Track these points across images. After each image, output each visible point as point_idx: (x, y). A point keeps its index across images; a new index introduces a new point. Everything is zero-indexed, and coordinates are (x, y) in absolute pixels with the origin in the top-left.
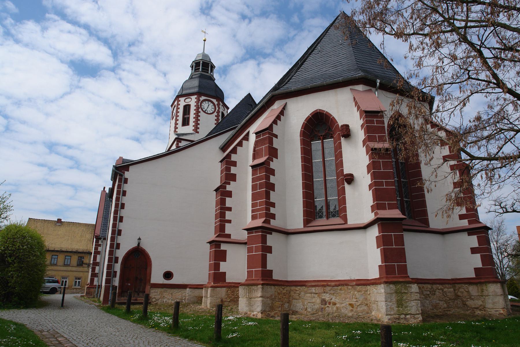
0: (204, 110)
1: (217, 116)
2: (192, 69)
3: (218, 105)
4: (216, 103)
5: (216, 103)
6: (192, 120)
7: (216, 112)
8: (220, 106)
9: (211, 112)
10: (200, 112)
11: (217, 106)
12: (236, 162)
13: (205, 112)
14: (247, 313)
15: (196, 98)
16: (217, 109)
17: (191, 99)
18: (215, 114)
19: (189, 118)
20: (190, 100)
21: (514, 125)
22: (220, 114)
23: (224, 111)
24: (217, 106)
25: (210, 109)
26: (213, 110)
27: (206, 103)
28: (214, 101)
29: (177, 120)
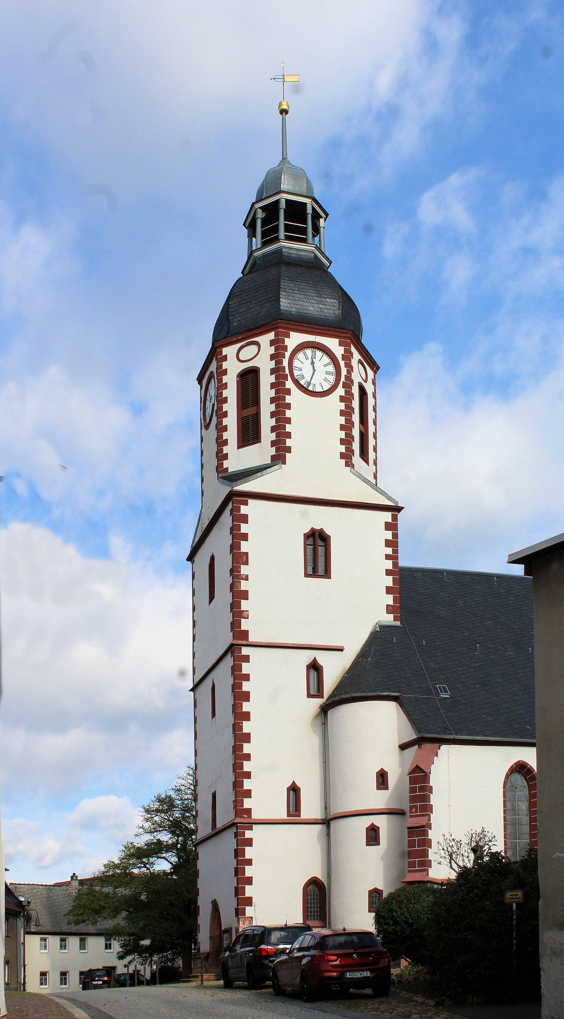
0: (302, 382)
1: (346, 399)
2: (252, 233)
3: (347, 357)
4: (339, 351)
5: (339, 351)
8: (354, 362)
9: (327, 387)
10: (288, 392)
11: (342, 363)
13: (304, 390)
15: (272, 343)
16: (344, 371)
17: (257, 344)
20: (254, 348)
22: (355, 390)
23: (366, 381)
24: (342, 363)
26: (332, 379)
27: (307, 358)
28: (332, 343)
29: (222, 429)
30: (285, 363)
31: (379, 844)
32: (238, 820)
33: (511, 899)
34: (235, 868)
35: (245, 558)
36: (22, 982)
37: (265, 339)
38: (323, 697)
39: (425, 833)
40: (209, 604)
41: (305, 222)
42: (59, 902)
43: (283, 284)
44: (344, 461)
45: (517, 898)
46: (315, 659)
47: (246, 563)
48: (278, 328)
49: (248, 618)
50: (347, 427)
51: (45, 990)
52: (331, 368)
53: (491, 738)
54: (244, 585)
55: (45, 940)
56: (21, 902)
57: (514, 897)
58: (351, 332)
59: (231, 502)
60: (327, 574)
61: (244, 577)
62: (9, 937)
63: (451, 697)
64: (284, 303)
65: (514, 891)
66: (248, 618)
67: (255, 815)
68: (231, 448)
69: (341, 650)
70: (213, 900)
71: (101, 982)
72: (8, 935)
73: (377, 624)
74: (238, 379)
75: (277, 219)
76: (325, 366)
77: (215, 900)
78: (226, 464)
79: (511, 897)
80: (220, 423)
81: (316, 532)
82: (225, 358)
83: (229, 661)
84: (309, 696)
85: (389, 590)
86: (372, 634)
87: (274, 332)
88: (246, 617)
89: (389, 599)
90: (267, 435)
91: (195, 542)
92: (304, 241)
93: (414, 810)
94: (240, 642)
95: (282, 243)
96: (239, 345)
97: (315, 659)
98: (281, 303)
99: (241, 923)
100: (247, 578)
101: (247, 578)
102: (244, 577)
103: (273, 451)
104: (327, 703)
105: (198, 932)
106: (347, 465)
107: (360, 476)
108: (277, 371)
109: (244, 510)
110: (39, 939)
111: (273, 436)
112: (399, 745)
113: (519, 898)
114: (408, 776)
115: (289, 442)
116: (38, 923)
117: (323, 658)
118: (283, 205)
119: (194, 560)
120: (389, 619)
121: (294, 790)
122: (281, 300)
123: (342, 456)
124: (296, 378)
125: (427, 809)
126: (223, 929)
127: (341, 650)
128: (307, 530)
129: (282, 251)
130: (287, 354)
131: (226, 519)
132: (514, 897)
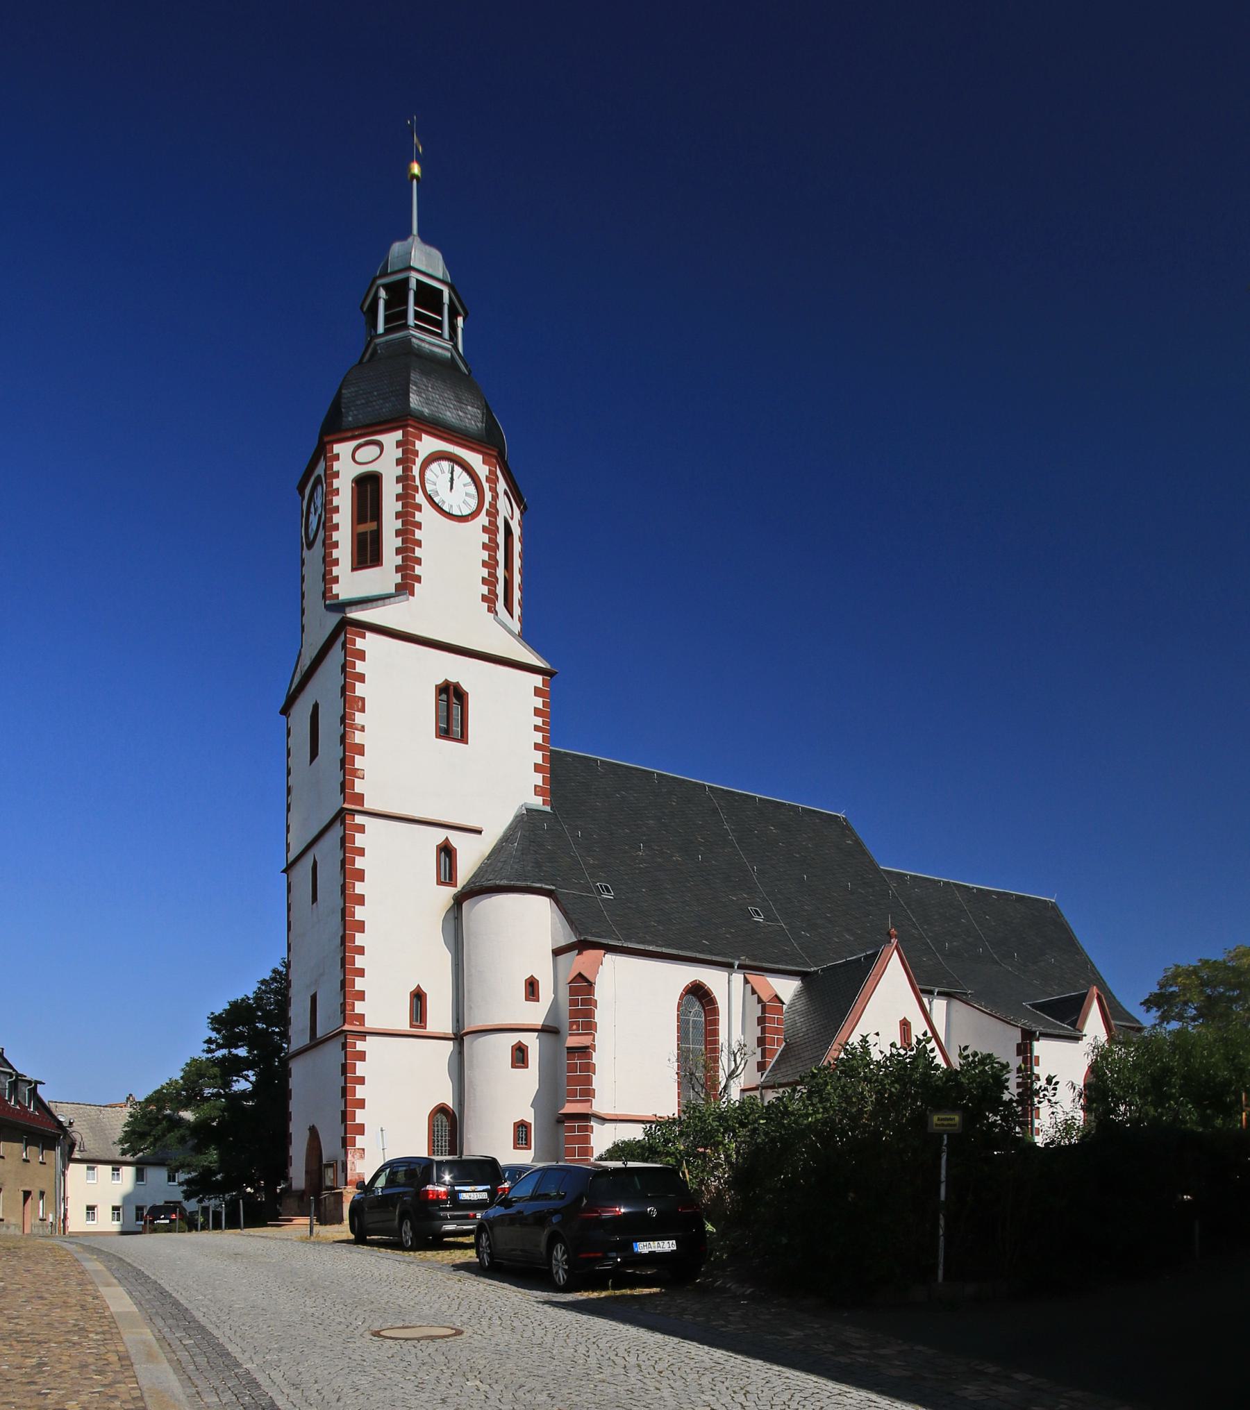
1: (490, 530)
5: (482, 471)
6: (390, 543)
7: (484, 511)
10: (419, 508)
11: (486, 486)
12: (364, 1100)
14: (522, 1212)
15: (399, 444)
16: (488, 496)
17: (380, 444)
18: (483, 519)
19: (377, 536)
20: (375, 450)
21: (199, 1348)
25: (460, 497)
26: (473, 503)
27: (443, 472)
28: (475, 459)
30: (416, 471)
31: (527, 1067)
32: (346, 1027)
33: (939, 1125)
34: (342, 1087)
35: (360, 704)
36: (62, 1217)
37: (390, 439)
38: (456, 886)
39: (589, 1056)
40: (310, 764)
41: (441, 315)
42: (111, 1125)
43: (414, 376)
44: (486, 604)
45: (951, 1125)
46: (447, 838)
47: (363, 710)
48: (407, 426)
49: (363, 778)
50: (490, 564)
51: (92, 1226)
52: (472, 490)
53: (664, 950)
54: (358, 738)
55: (118, 1170)
56: (60, 1123)
57: (946, 1123)
58: (497, 450)
59: (343, 633)
60: (463, 738)
61: (359, 727)
62: (45, 1163)
63: (615, 898)
64: (414, 401)
65: (945, 1112)
66: (363, 778)
67: (370, 1024)
68: (343, 569)
69: (479, 832)
70: (311, 1125)
71: (168, 1221)
72: (44, 1161)
73: (522, 806)
74: (353, 485)
75: (406, 303)
76: (465, 485)
77: (313, 1126)
78: (336, 589)
79: (939, 1123)
80: (328, 537)
81: (450, 685)
82: (337, 457)
83: (337, 831)
84: (440, 883)
85: (538, 768)
86: (516, 817)
87: (401, 431)
88: (362, 777)
89: (538, 779)
90: (390, 557)
91: (293, 687)
92: (440, 336)
93: (574, 1027)
94: (353, 807)
95: (411, 332)
96: (354, 443)
97: (447, 838)
98: (411, 399)
99: (350, 1156)
100: (362, 729)
101: (362, 729)
102: (359, 727)
103: (398, 578)
104: (463, 891)
105: (289, 1164)
106: (489, 610)
107: (504, 626)
108: (405, 479)
109: (360, 644)
110: (86, 1169)
111: (398, 560)
112: (552, 950)
113: (955, 1125)
114: (568, 986)
115: (418, 570)
116: (82, 1149)
117: (456, 839)
118: (413, 285)
119: (290, 714)
120: (537, 802)
121: (418, 997)
122: (411, 395)
123: (484, 598)
124: (429, 493)
125: (589, 1027)
126: (324, 1162)
127: (479, 832)
128: (440, 681)
129: (411, 341)
130: (419, 461)
131: (336, 654)
132: (946, 1123)
